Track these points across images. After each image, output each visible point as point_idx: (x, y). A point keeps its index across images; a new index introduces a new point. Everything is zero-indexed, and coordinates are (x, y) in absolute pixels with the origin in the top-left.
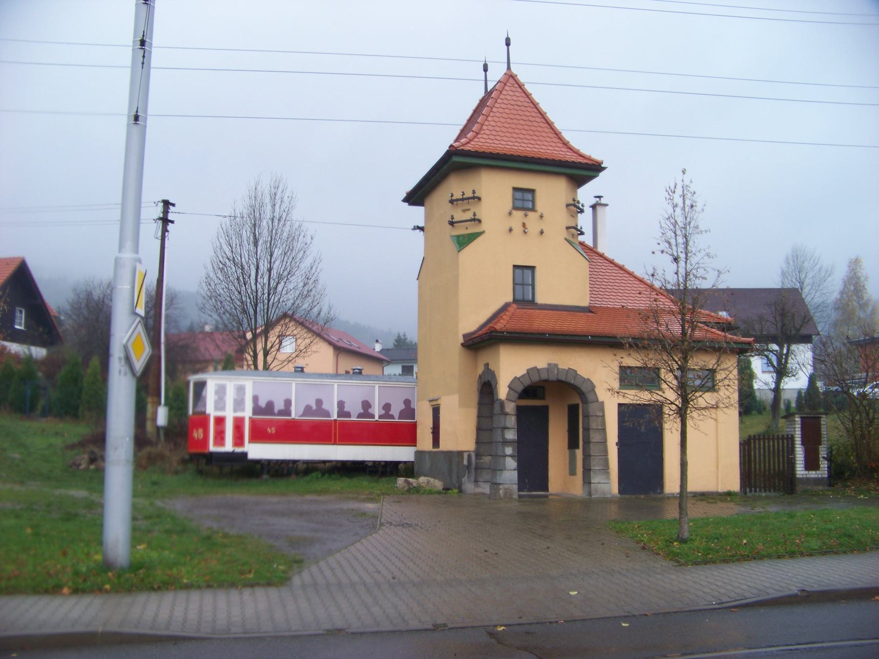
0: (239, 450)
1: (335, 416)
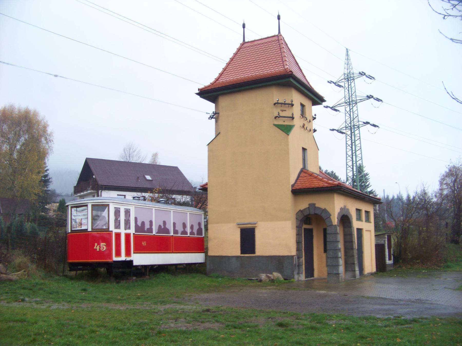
0: (128, 259)
1: (172, 234)
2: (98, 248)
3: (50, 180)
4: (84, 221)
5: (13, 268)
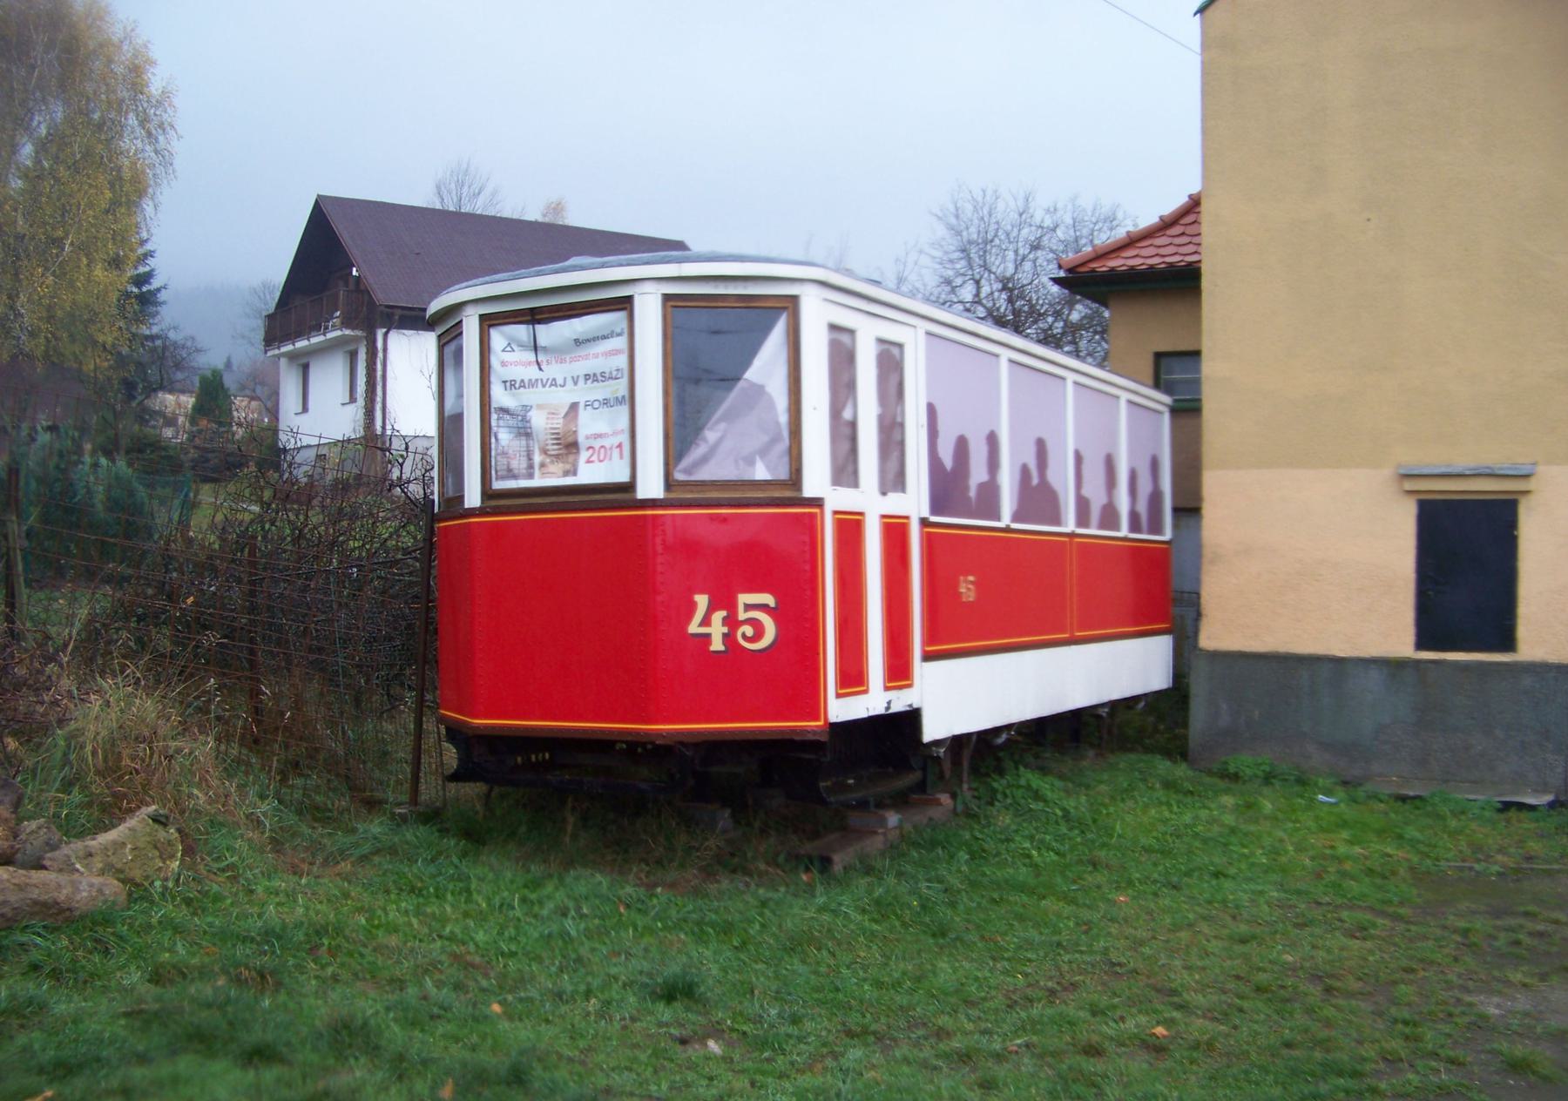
0: (900, 701)
1: (1070, 526)
2: (717, 630)
3: (162, 296)
4: (589, 425)
5: (67, 786)
